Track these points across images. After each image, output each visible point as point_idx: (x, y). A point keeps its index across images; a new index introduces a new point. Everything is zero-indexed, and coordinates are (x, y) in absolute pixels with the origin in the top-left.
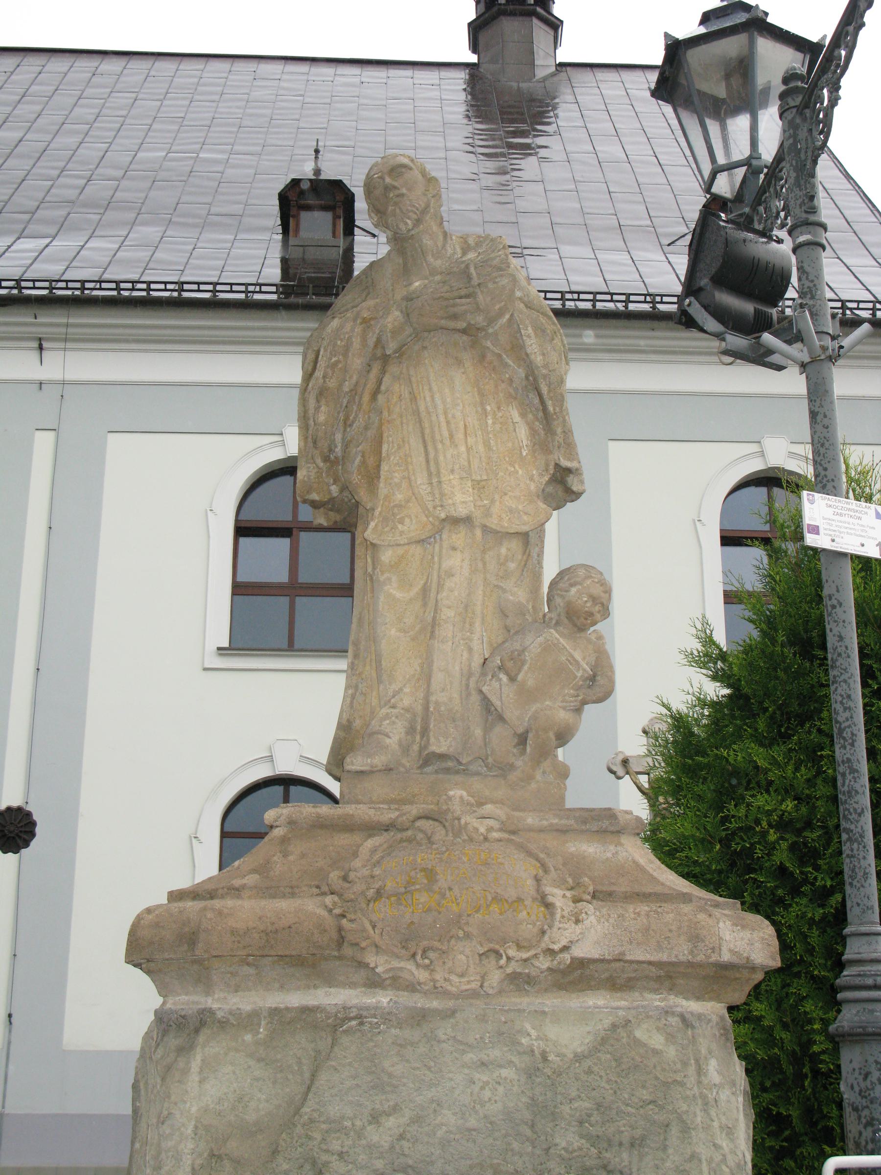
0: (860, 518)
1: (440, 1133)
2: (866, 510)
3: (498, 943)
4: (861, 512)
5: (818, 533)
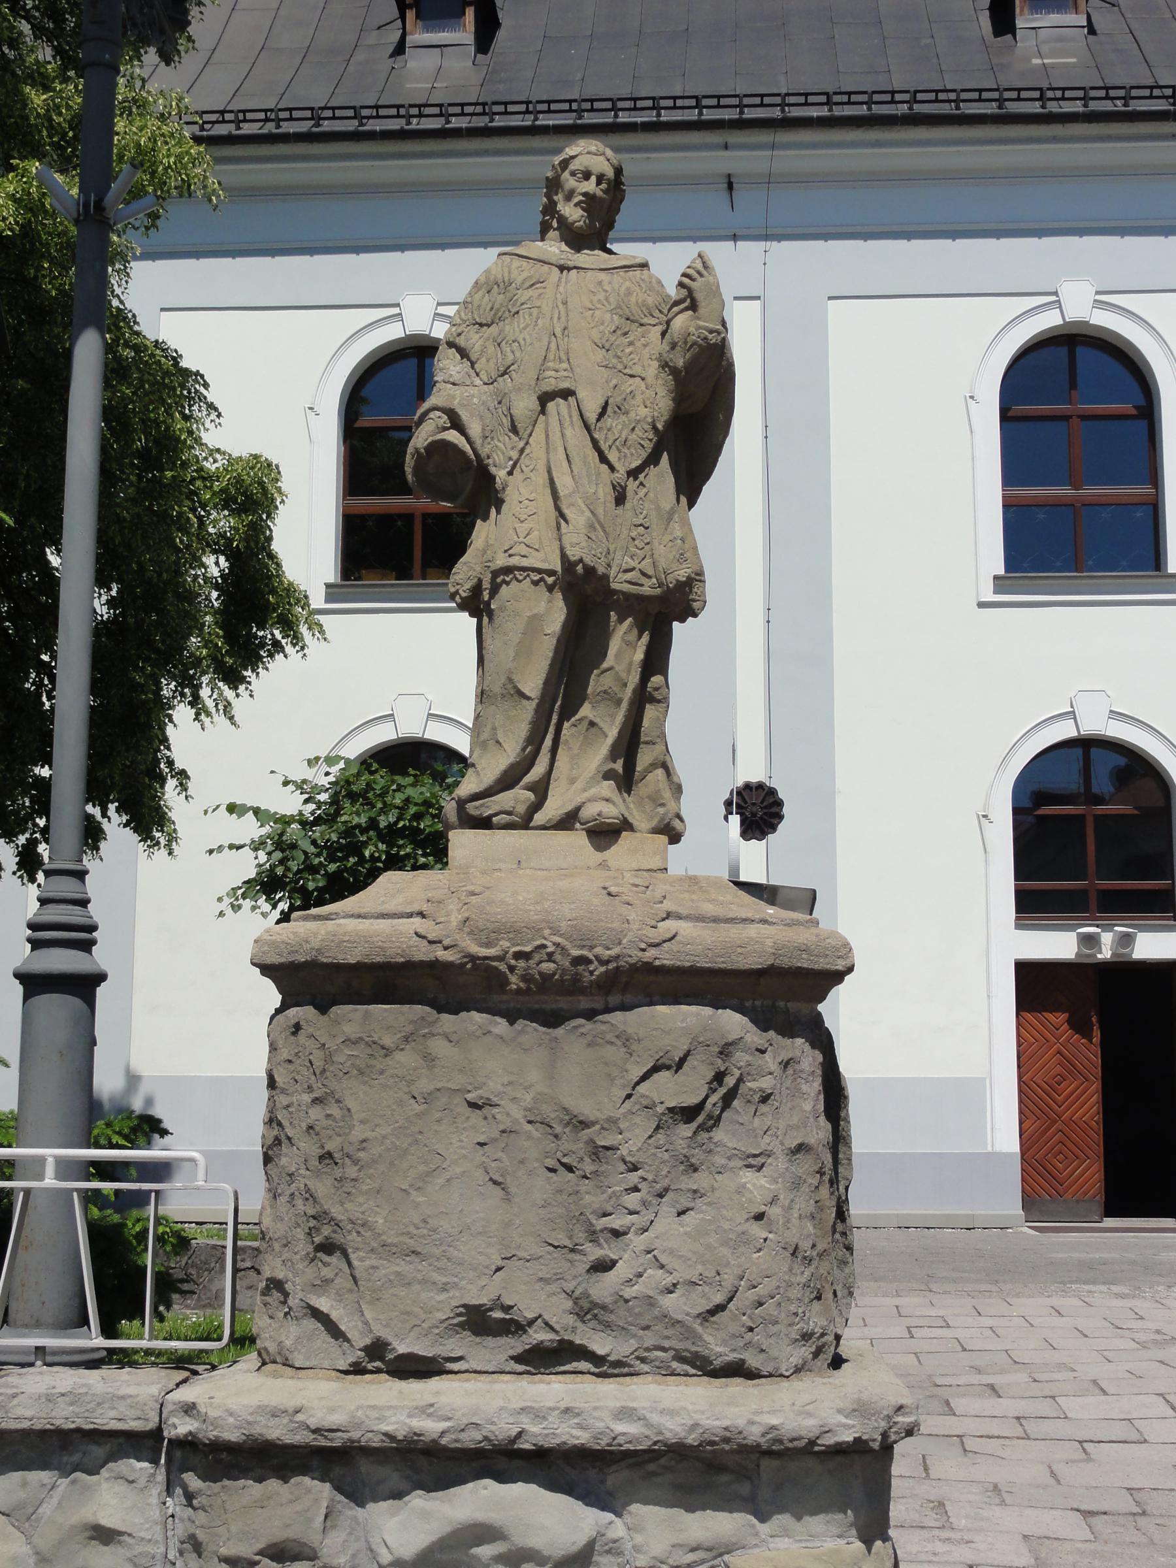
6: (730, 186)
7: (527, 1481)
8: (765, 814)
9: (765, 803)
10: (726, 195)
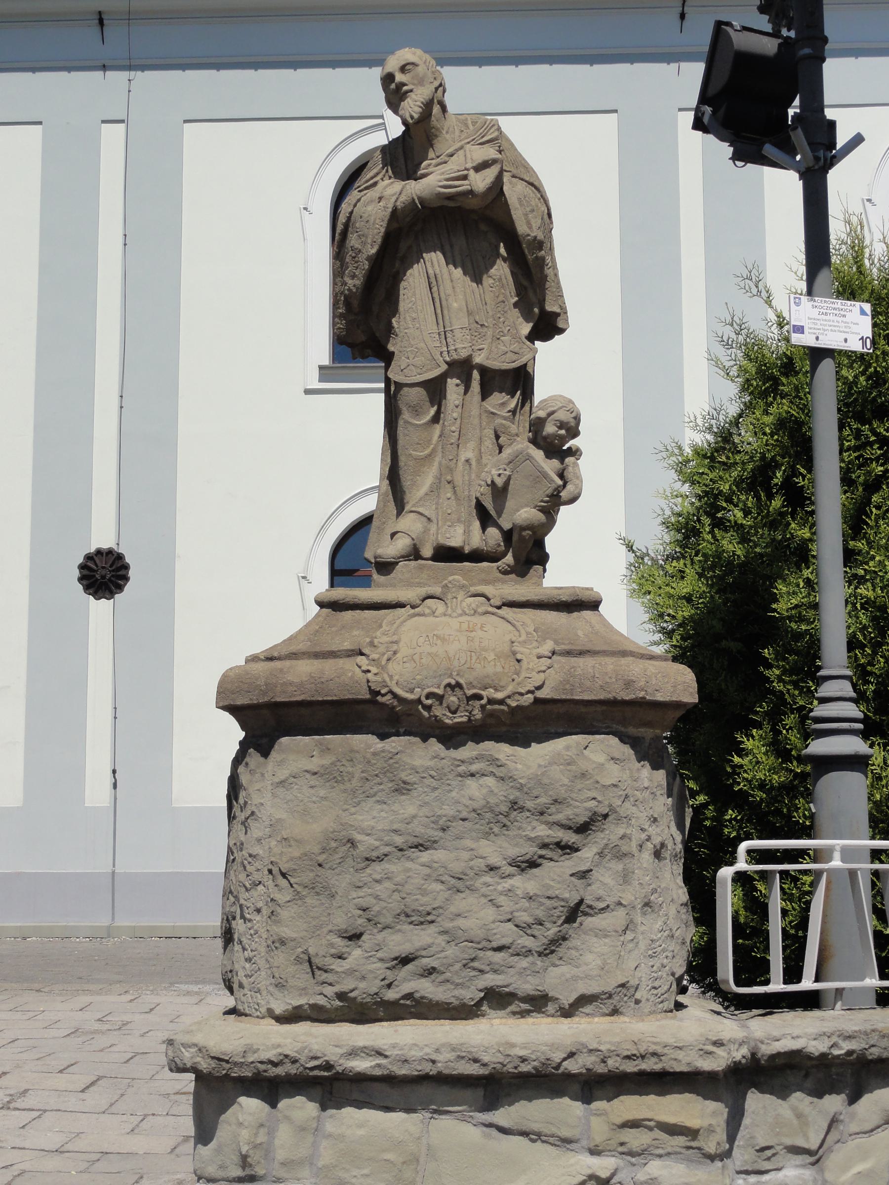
0: (844, 316)
1: (441, 822)
2: (851, 308)
3: (480, 689)
4: (845, 310)
5: (803, 333)
6: (101, 22)
7: (690, 1093)
8: (113, 576)
9: (114, 567)
10: (97, 29)
